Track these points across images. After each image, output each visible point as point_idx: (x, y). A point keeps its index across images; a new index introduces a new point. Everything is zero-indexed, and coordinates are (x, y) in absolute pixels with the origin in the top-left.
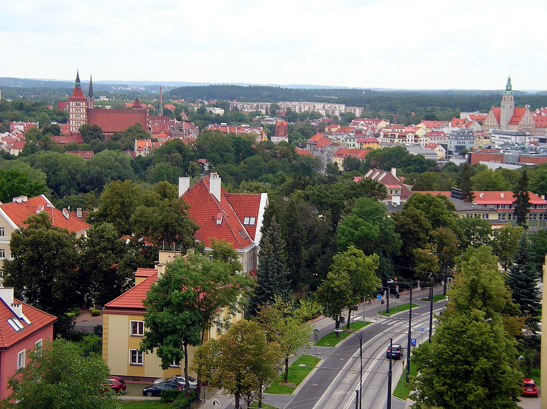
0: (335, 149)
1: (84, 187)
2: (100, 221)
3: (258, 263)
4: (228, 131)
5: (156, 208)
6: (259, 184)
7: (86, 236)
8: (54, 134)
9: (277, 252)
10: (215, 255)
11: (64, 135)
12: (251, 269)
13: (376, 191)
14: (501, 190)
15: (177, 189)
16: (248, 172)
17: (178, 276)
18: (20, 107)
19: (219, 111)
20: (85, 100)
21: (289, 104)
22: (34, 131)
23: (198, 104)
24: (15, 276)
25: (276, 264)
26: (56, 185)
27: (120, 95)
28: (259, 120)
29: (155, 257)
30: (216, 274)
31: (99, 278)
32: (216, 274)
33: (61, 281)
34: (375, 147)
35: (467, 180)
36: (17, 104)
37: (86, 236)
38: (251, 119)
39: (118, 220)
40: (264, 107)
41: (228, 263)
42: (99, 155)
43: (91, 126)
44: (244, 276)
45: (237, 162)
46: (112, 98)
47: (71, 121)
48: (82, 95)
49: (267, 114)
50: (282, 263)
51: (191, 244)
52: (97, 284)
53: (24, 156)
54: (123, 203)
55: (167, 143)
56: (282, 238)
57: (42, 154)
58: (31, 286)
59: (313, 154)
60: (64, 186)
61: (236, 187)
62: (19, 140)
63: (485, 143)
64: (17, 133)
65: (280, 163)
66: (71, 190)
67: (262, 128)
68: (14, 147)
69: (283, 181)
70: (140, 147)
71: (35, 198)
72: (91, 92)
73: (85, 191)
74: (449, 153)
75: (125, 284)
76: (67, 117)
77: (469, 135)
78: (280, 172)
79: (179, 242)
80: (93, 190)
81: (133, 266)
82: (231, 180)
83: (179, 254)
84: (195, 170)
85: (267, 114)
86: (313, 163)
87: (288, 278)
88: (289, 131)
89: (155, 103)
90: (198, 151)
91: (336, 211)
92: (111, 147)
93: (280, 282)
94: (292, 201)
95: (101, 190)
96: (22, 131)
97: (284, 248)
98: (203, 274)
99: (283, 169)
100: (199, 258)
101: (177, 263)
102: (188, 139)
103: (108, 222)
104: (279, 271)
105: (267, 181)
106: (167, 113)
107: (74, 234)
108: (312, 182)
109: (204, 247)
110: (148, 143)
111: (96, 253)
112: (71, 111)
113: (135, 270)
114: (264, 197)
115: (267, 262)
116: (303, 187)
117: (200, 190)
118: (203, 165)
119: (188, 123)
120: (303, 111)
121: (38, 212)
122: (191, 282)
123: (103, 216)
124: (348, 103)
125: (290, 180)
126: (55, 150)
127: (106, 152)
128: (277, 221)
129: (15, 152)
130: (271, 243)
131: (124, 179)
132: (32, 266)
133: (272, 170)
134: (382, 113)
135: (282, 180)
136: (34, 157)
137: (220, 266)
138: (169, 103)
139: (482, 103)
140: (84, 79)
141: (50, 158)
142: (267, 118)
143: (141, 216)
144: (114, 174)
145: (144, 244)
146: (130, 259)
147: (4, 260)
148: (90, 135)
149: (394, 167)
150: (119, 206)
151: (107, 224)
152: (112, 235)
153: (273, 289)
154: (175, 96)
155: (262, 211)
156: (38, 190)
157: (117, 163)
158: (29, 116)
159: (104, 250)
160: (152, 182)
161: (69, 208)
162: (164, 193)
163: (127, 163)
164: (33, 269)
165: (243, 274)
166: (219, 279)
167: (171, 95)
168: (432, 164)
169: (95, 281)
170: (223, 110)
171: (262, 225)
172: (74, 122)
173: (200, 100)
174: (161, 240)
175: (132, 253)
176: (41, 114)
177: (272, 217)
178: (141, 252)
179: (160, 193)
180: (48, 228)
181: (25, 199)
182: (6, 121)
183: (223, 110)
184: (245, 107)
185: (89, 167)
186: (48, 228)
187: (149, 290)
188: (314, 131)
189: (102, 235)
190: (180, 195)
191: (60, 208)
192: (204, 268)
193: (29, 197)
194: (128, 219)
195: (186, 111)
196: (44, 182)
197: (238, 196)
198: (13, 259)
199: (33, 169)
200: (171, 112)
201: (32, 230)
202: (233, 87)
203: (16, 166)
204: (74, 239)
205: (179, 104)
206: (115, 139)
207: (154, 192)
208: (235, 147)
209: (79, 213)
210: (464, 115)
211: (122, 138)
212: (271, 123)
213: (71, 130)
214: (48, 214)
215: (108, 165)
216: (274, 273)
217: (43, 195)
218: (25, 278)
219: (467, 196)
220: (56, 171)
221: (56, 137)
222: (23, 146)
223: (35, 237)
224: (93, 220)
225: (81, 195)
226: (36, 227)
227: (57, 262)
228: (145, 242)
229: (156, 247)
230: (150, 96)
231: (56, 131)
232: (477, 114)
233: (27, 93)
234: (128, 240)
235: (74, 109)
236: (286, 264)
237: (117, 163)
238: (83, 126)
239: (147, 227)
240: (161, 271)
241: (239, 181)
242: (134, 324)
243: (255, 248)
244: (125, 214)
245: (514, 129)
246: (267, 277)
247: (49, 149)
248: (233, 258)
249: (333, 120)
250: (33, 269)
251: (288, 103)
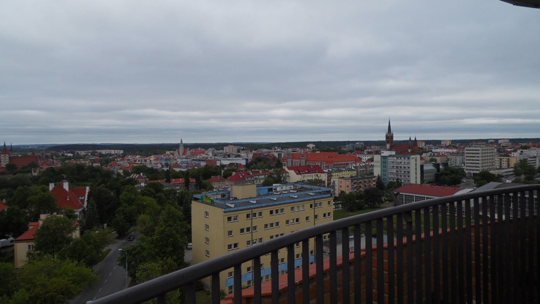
0: (119, 167)
14: (180, 178)
34: (135, 165)
35: (169, 175)
63: (174, 162)
69: (97, 181)
77: (169, 159)
81: (28, 220)
91: (118, 193)
106: (47, 157)
114: (88, 188)
124: (268, 148)
125: (100, 180)
134: (137, 152)
139: (174, 147)
149: (51, 182)
155: (87, 194)
168: (157, 170)
188: (111, 160)
210: (168, 152)
219: (168, 181)
232: (172, 152)
240: (41, 223)
242: (29, 246)
245: (184, 157)
249: (118, 156)
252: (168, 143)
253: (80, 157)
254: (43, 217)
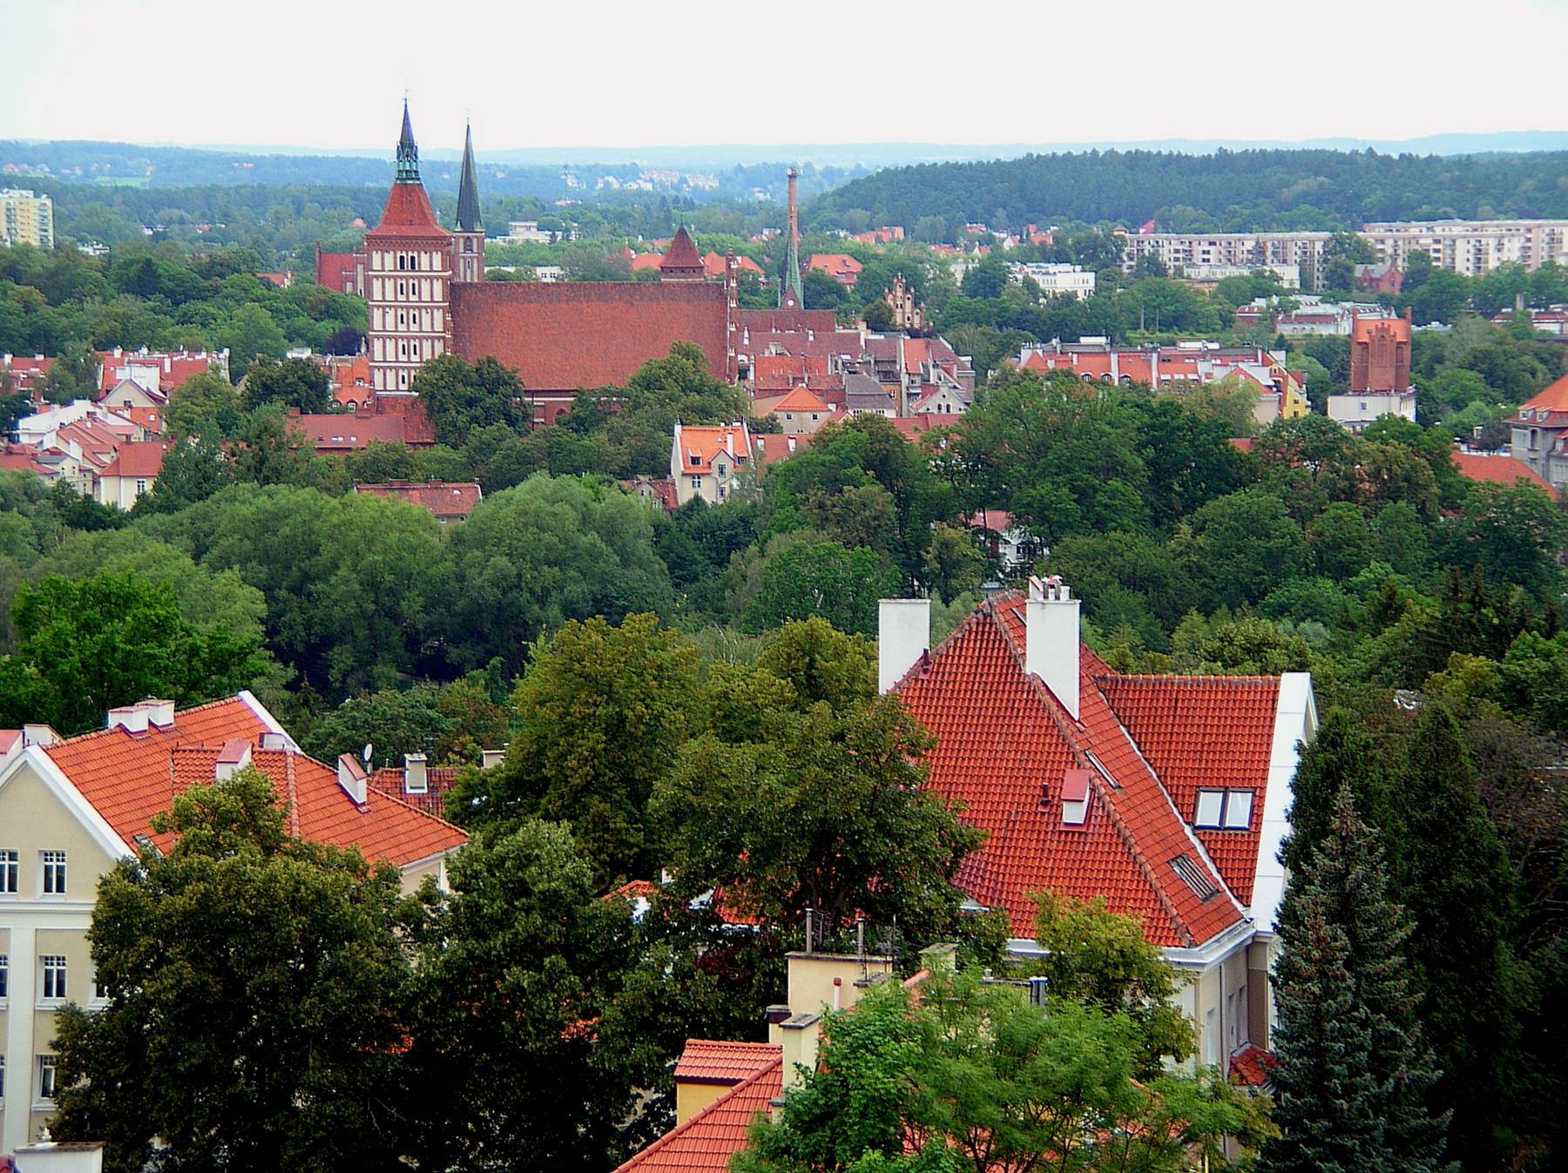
1: (440, 653)
2: (512, 812)
3: (1272, 1019)
4: (1115, 374)
5: (771, 746)
6: (1266, 627)
7: (444, 886)
8: (296, 403)
9: (1370, 968)
10: (1059, 975)
11: (343, 411)
12: (1238, 1045)
15: (871, 657)
16: (1213, 571)
17: (877, 1079)
18: (143, 279)
19: (1073, 281)
20: (438, 242)
21: (1420, 234)
22: (208, 392)
23: (968, 249)
24: (110, 1089)
25: (1364, 1024)
26: (308, 643)
27: (604, 214)
28: (1270, 318)
29: (769, 986)
30: (1064, 1069)
31: (504, 1087)
32: (1064, 1069)
33: (329, 1109)
36: (127, 265)
37: (444, 886)
38: (1227, 316)
39: (597, 805)
40: (1294, 253)
41: (1122, 1018)
42: (509, 500)
43: (470, 365)
44: (1205, 1084)
45: (1157, 523)
46: (567, 230)
47: (378, 345)
48: (425, 220)
49: (1306, 286)
50: (1398, 1022)
51: (942, 920)
52: (495, 1117)
53: (160, 509)
54: (615, 728)
55: (822, 440)
56: (1391, 894)
57: (245, 502)
58: (188, 1131)
59: (1546, 473)
60: (343, 651)
61: (1157, 644)
62: (138, 435)
64: (128, 405)
65: (1376, 523)
66: (378, 669)
67: (1280, 356)
68: (116, 471)
69: (1389, 611)
70: (695, 461)
71: (211, 711)
72: (467, 206)
73: (443, 671)
75: (629, 1120)
76: (358, 324)
78: (1377, 569)
79: (882, 910)
80: (481, 665)
81: (664, 1028)
82: (1132, 610)
83: (881, 970)
84: (957, 564)
85: (1306, 286)
86: (1545, 522)
87: (1435, 1097)
88: (1419, 367)
89: (766, 249)
90: (971, 472)
92: (561, 462)
93: (1393, 1119)
94: (1437, 712)
95: (516, 664)
96: (150, 394)
97: (1404, 947)
98: (1002, 1072)
99: (1393, 553)
100: (980, 993)
101: (871, 1015)
102: (924, 417)
103: (547, 817)
104: (1384, 1062)
105: (1312, 611)
106: (821, 293)
107: (390, 877)
108: (1539, 617)
109: (1001, 940)
110: (733, 441)
111: (491, 966)
112: (377, 295)
113: (678, 1051)
114: (1295, 692)
115: (1318, 1018)
116: (1497, 642)
118: (995, 537)
119: (921, 342)
120: (1493, 263)
121: (223, 773)
122: (944, 1109)
123: (523, 791)
126: (307, 481)
127: (537, 486)
128: (1364, 809)
129: (120, 494)
130: (1333, 917)
131: (624, 611)
132: (193, 1038)
133: (1336, 562)
135: (1387, 607)
136: (206, 517)
137: (1079, 1032)
138: (832, 246)
140: (438, 146)
141: (280, 516)
142: (1309, 305)
143: (699, 786)
144: (577, 590)
145: (720, 922)
146: (650, 995)
147: (59, 1011)
148: (467, 406)
150: (596, 738)
151: (545, 827)
152: (567, 878)
153: (1359, 1157)
154: (860, 215)
156: (223, 669)
157: (593, 537)
158: (185, 320)
159: (529, 951)
160: (755, 626)
161: (368, 751)
162: (809, 677)
163: (638, 535)
164: (197, 1052)
165: (1200, 1073)
166: (1075, 1095)
167: (842, 209)
169: (489, 1105)
170: (1091, 276)
171: (1287, 830)
172: (390, 345)
173: (979, 229)
174: (799, 900)
175: (661, 963)
176: (238, 312)
177: (1335, 789)
178: (704, 963)
179: (787, 673)
180: (268, 851)
181: (164, 713)
182: (79, 350)
183: (1091, 276)
184: (1198, 257)
185: (460, 556)
186: (268, 851)
187: (740, 1148)
189: (522, 882)
190: (885, 684)
191: (323, 752)
192: (1005, 1041)
193: (181, 703)
194: (640, 795)
195: (914, 282)
196: (252, 631)
197: (1160, 688)
198: (104, 1002)
199: (202, 571)
200: (839, 291)
201: (194, 859)
202: (1137, 161)
203: (127, 558)
204: (390, 903)
205: (881, 250)
206: (581, 425)
207: (764, 674)
208: (1150, 452)
209: (416, 776)
211: (614, 421)
212: (1326, 331)
213: (379, 385)
214: (268, 781)
215: (550, 548)
216: (1355, 1071)
217: (246, 696)
218: (157, 1096)
220: (307, 577)
221: (310, 419)
222: (156, 465)
223: (206, 895)
224: (479, 811)
225: (423, 691)
226: (215, 848)
227: (310, 1013)
228: (723, 911)
229: (774, 938)
230: (742, 217)
231: (309, 393)
232: (1348, 305)
233: (176, 213)
234: (642, 906)
235: (389, 284)
236: (1417, 1029)
237: (593, 537)
238: (430, 367)
239: (727, 840)
240: (797, 1051)
241: (1170, 617)
243: (1254, 946)
244: (628, 780)
246: (1324, 1094)
247: (277, 476)
248: (1147, 992)
250: (197, 1052)
251: (1415, 229)
252: (1512, 151)
253: (1172, 313)
254: (817, 987)
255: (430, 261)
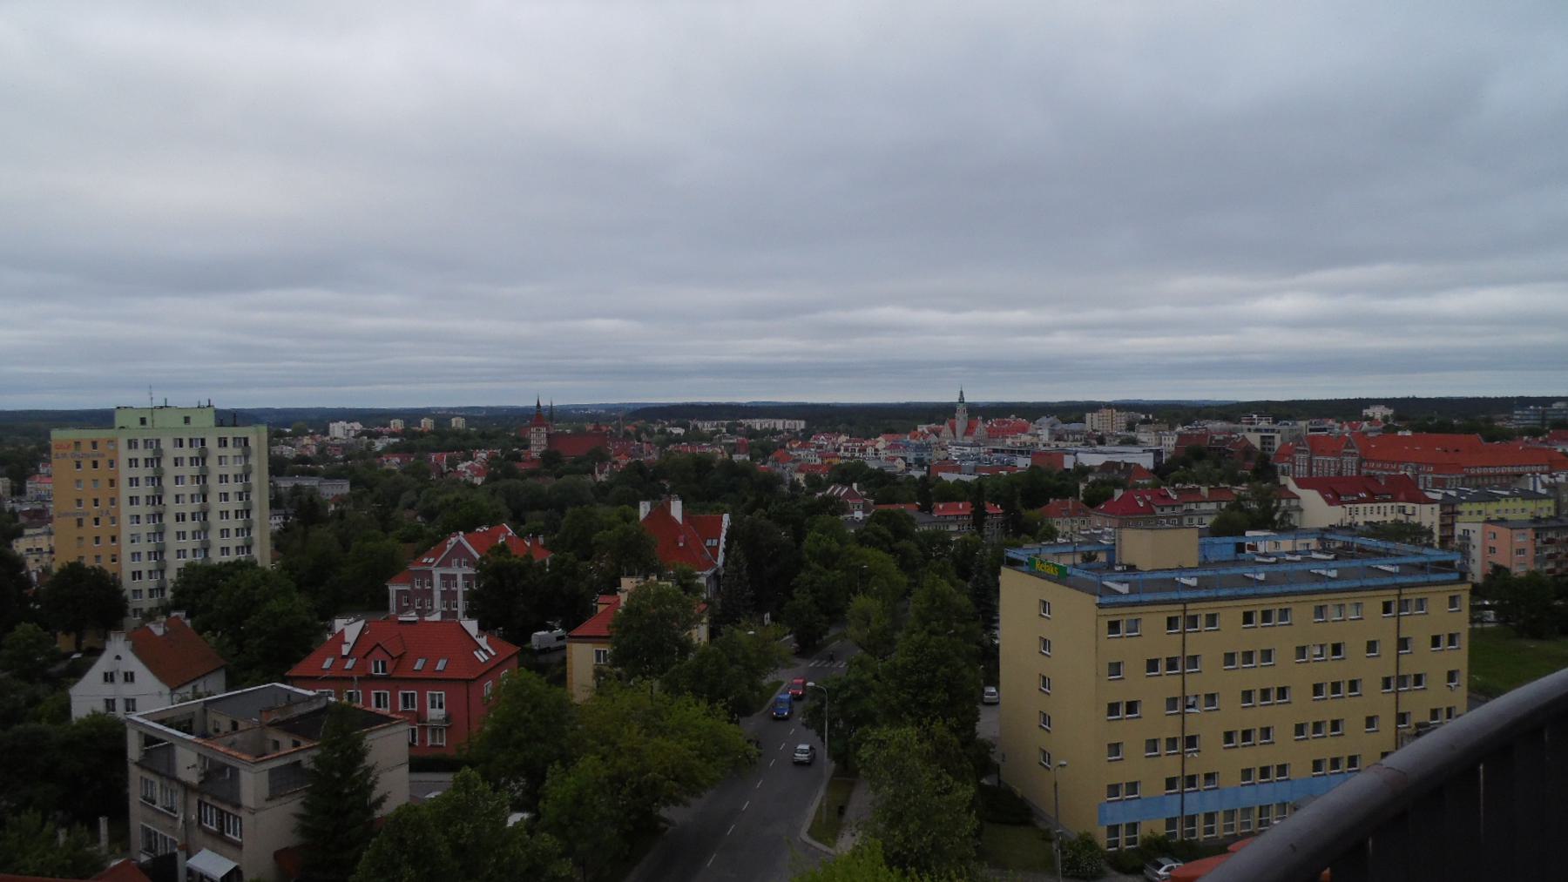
0: (801, 462)
13: (835, 507)
18: (483, 436)
34: (836, 461)
35: (929, 492)
63: (942, 455)
69: (744, 500)
74: (908, 465)
77: (927, 447)
88: (749, 449)
114: (726, 517)
117: (662, 512)
125: (751, 499)
129: (478, 481)
139: (939, 414)
148: (550, 459)
168: (892, 476)
188: (775, 448)
209: (541, 540)
210: (922, 428)
219: (926, 508)
232: (933, 426)
242: (598, 653)
245: (969, 440)
249: (794, 436)
253: (702, 438)
254: (627, 583)
255: (544, 430)
